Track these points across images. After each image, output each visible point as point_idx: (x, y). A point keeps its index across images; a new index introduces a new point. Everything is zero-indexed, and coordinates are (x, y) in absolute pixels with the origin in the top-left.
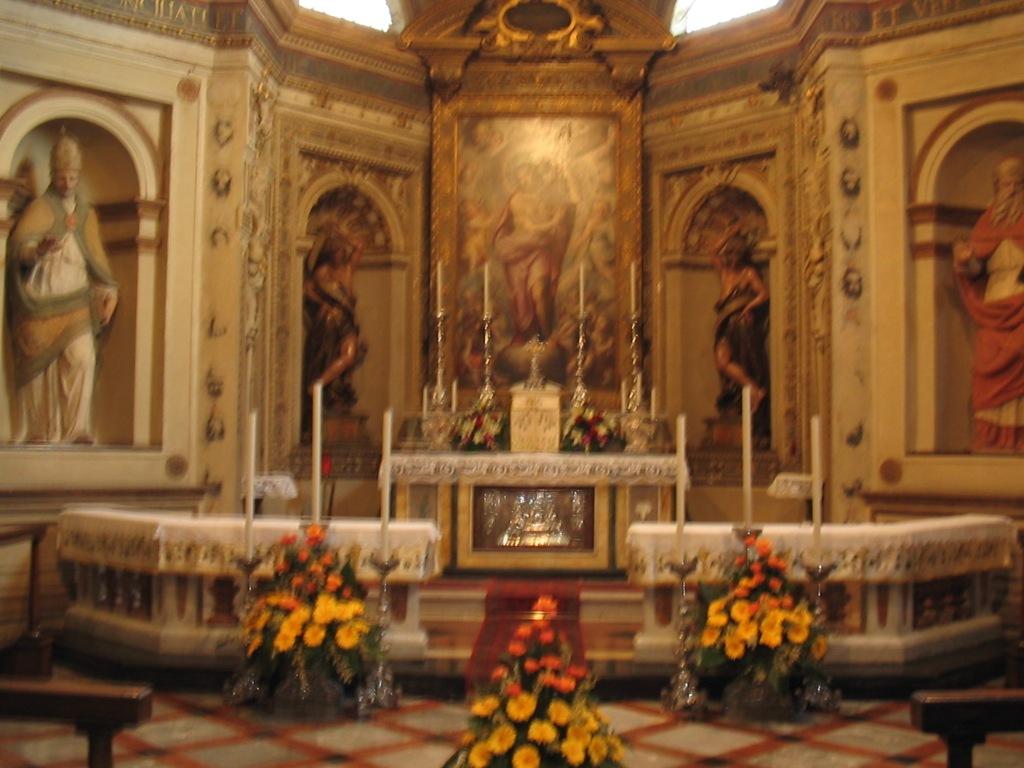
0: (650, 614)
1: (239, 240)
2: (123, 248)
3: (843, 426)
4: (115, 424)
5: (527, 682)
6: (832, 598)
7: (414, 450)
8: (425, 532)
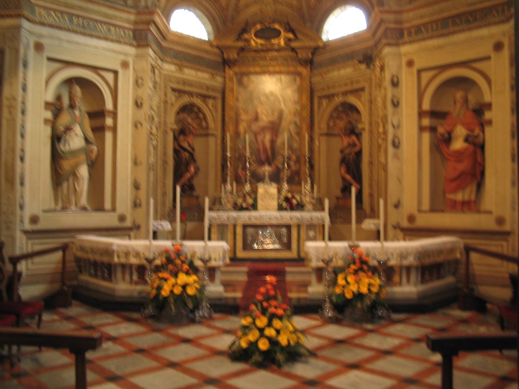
0: (313, 278)
1: (146, 126)
2: (99, 130)
3: (392, 200)
4: (97, 204)
5: (264, 311)
6: (387, 272)
7: (219, 210)
8: (223, 247)
